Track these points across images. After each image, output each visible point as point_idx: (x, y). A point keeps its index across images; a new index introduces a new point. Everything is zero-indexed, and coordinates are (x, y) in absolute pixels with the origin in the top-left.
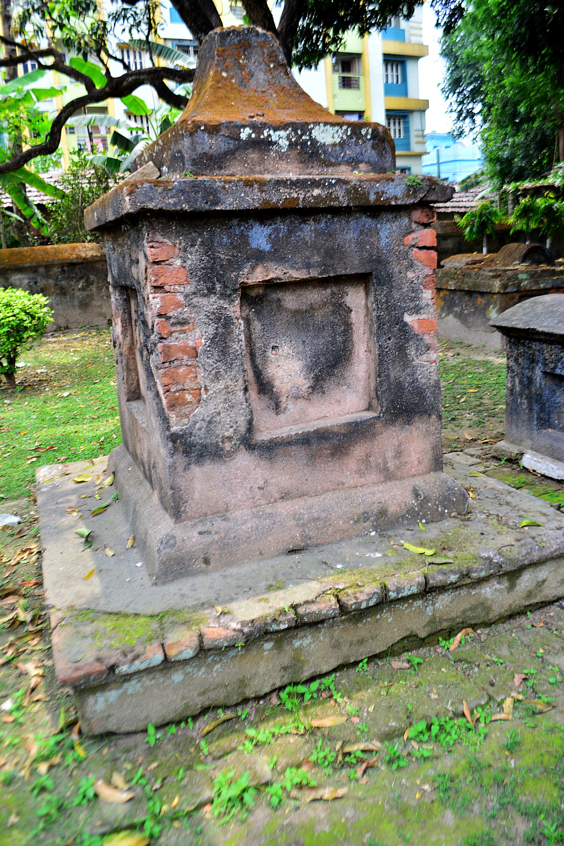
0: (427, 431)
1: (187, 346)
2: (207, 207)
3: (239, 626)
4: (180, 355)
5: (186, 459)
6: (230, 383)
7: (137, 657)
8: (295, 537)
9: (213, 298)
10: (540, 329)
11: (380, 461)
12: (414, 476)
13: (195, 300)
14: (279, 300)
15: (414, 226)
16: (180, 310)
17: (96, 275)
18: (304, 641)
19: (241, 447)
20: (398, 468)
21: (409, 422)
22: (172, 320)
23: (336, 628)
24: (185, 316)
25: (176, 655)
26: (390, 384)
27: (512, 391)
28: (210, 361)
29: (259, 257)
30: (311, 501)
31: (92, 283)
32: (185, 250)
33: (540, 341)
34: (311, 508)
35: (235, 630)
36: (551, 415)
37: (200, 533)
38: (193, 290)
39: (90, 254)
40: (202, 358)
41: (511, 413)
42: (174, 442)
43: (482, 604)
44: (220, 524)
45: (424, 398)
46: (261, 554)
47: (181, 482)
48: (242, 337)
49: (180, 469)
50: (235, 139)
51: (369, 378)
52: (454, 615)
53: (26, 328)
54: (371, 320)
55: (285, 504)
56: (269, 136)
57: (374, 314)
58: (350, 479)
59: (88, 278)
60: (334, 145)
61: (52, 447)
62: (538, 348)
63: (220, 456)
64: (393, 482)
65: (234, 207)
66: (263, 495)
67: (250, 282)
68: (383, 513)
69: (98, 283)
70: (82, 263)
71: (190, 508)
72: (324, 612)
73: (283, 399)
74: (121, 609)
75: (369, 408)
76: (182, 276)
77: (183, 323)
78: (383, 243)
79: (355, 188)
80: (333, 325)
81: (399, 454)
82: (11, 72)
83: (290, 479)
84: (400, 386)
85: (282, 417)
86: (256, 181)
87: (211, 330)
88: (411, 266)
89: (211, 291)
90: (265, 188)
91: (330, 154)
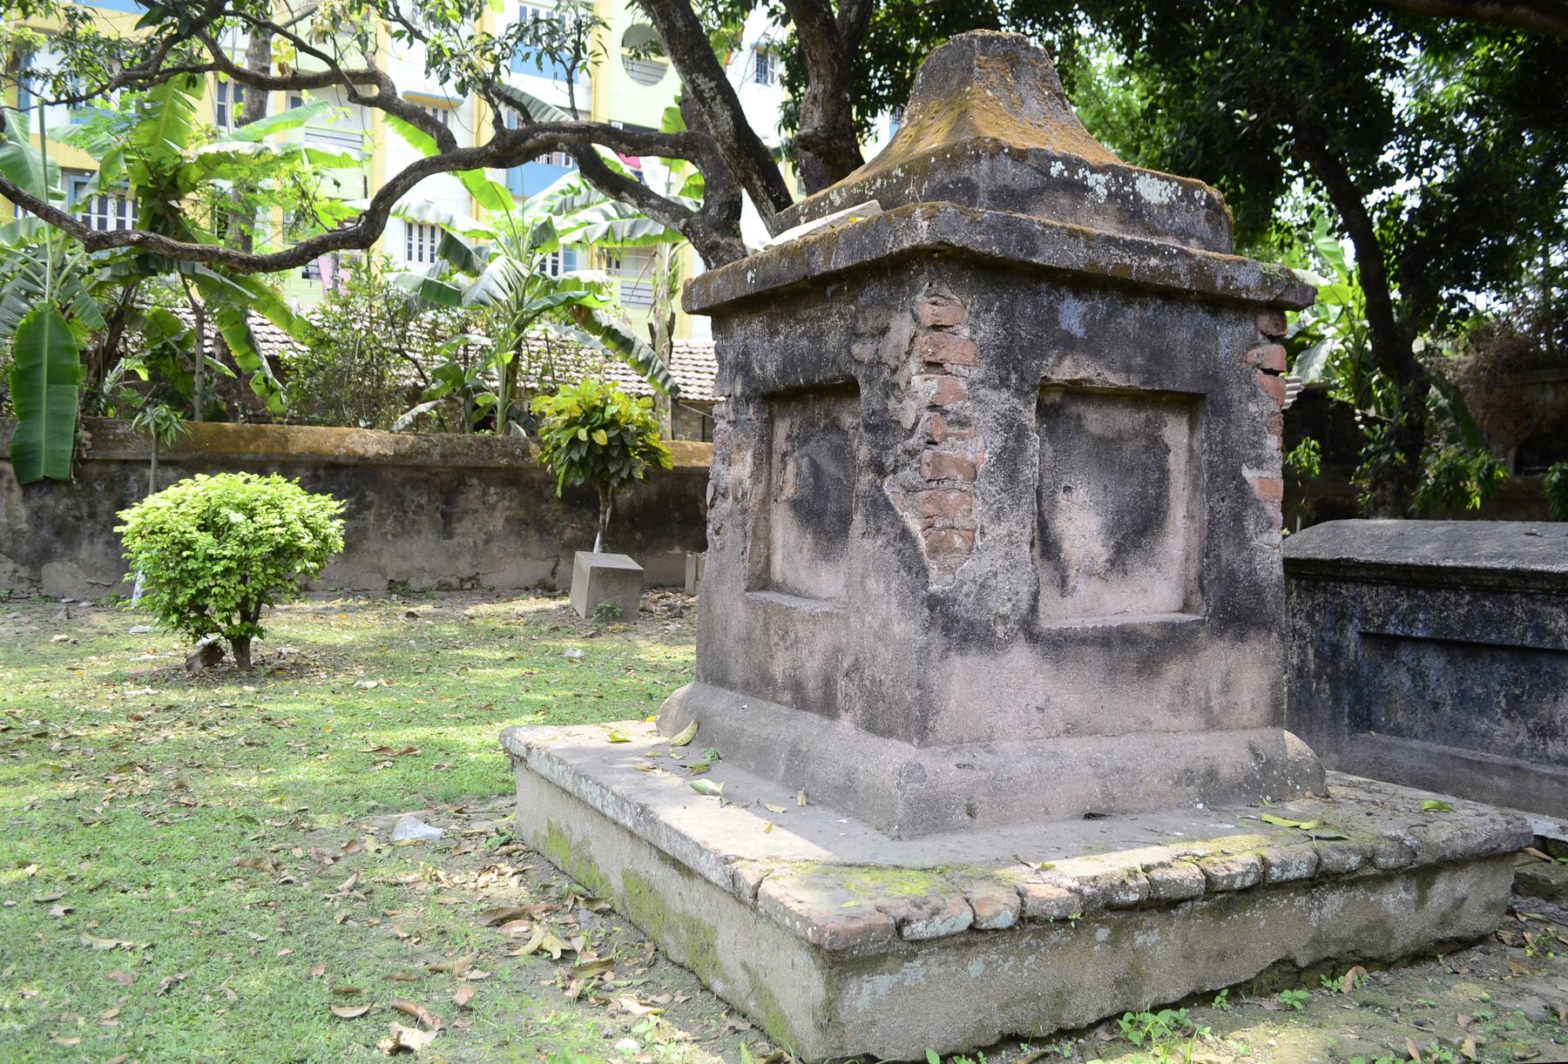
0: (1265, 656)
1: (964, 460)
2: (1021, 256)
3: (1075, 885)
4: (953, 472)
5: (945, 640)
6: (1015, 528)
7: (936, 912)
8: (1091, 793)
9: (1005, 394)
10: (1362, 559)
11: (1201, 694)
12: (1245, 728)
13: (982, 392)
14: (1079, 417)
15: (1260, 336)
16: (960, 403)
17: (378, 492)
18: (1151, 938)
19: (1021, 635)
20: (1226, 710)
21: (1241, 637)
22: (950, 417)
23: (1192, 922)
24: (968, 413)
25: (992, 918)
26: (1220, 572)
27: (1300, 671)
28: (993, 489)
29: (1069, 344)
30: (1108, 743)
31: (369, 507)
32: (977, 316)
33: (1355, 581)
34: (1110, 752)
35: (1070, 890)
36: (1373, 709)
37: (958, 766)
38: (981, 376)
39: (372, 450)
40: (982, 483)
41: (1298, 710)
42: (932, 609)
43: (1382, 922)
44: (982, 757)
45: (1262, 602)
46: (1047, 812)
47: (934, 678)
48: (1036, 460)
49: (935, 655)
50: (1040, 172)
51: (1187, 559)
52: (1344, 934)
53: (301, 552)
54: (1199, 468)
55: (1071, 741)
56: (1085, 177)
57: (1205, 458)
58: (1162, 720)
59: (363, 495)
60: (1161, 206)
61: (411, 750)
62: (1352, 593)
63: (991, 645)
64: (1218, 733)
65: (1052, 263)
66: (1042, 722)
67: (1054, 378)
68: (1212, 774)
69: (381, 506)
70: (355, 466)
71: (942, 724)
72: (1187, 882)
73: (1072, 572)
74: (867, 860)
75: (1186, 608)
76: (970, 353)
77: (963, 423)
78: (1222, 355)
79: (1199, 263)
80: (1145, 467)
81: (1227, 687)
82: (255, 107)
83: (1081, 701)
84: (1232, 576)
85: (1069, 601)
86: (1083, 233)
87: (998, 441)
88: (1254, 395)
89: (1004, 383)
90: (1092, 244)
91: (1155, 217)
